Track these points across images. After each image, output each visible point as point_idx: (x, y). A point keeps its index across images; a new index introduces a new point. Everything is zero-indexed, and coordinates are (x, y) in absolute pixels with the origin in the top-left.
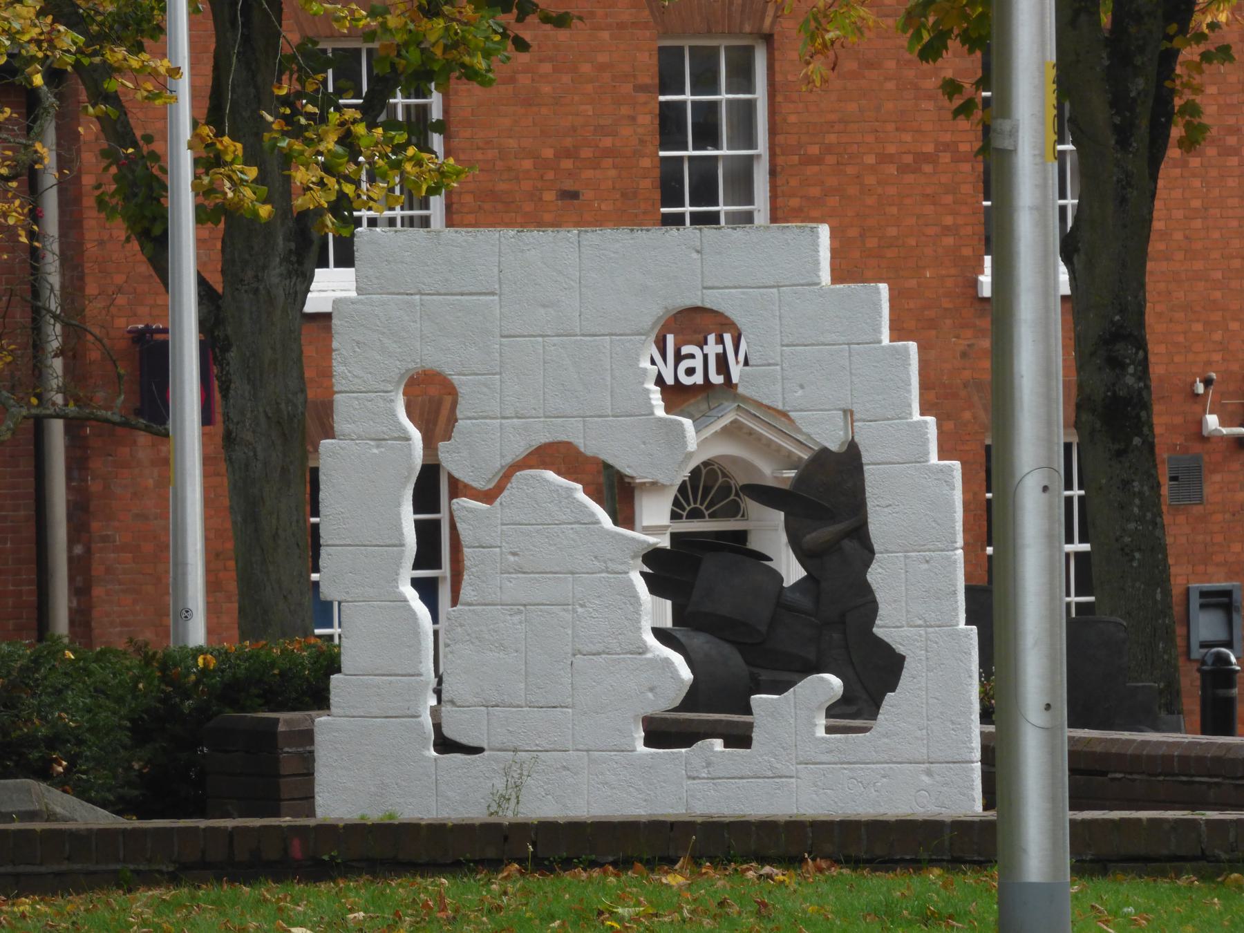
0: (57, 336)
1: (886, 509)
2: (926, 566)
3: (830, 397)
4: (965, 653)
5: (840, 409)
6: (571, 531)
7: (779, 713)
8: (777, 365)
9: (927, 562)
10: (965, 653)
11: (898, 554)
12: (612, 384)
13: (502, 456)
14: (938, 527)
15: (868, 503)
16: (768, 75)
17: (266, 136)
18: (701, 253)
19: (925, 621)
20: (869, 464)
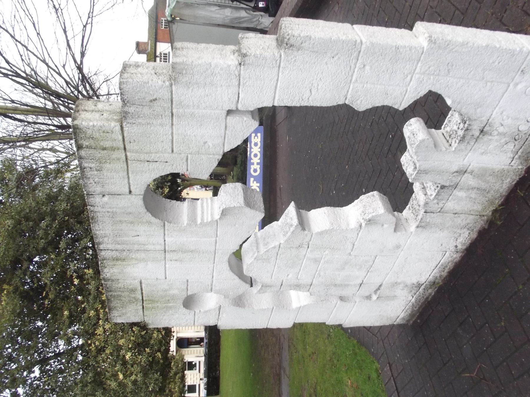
0: (92, 18)
1: (313, 93)
2: (367, 68)
3: (215, 124)
4: (448, 45)
5: (226, 119)
6: (282, 256)
7: (442, 166)
8: (187, 156)
9: (364, 66)
10: (448, 45)
11: (351, 87)
12: (269, 249)
13: (234, 279)
14: (339, 55)
15: (305, 105)
16: (218, 357)
17: (68, 273)
18: (417, 14)
19: (409, 73)
20: (274, 102)
